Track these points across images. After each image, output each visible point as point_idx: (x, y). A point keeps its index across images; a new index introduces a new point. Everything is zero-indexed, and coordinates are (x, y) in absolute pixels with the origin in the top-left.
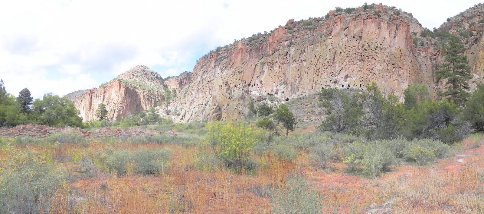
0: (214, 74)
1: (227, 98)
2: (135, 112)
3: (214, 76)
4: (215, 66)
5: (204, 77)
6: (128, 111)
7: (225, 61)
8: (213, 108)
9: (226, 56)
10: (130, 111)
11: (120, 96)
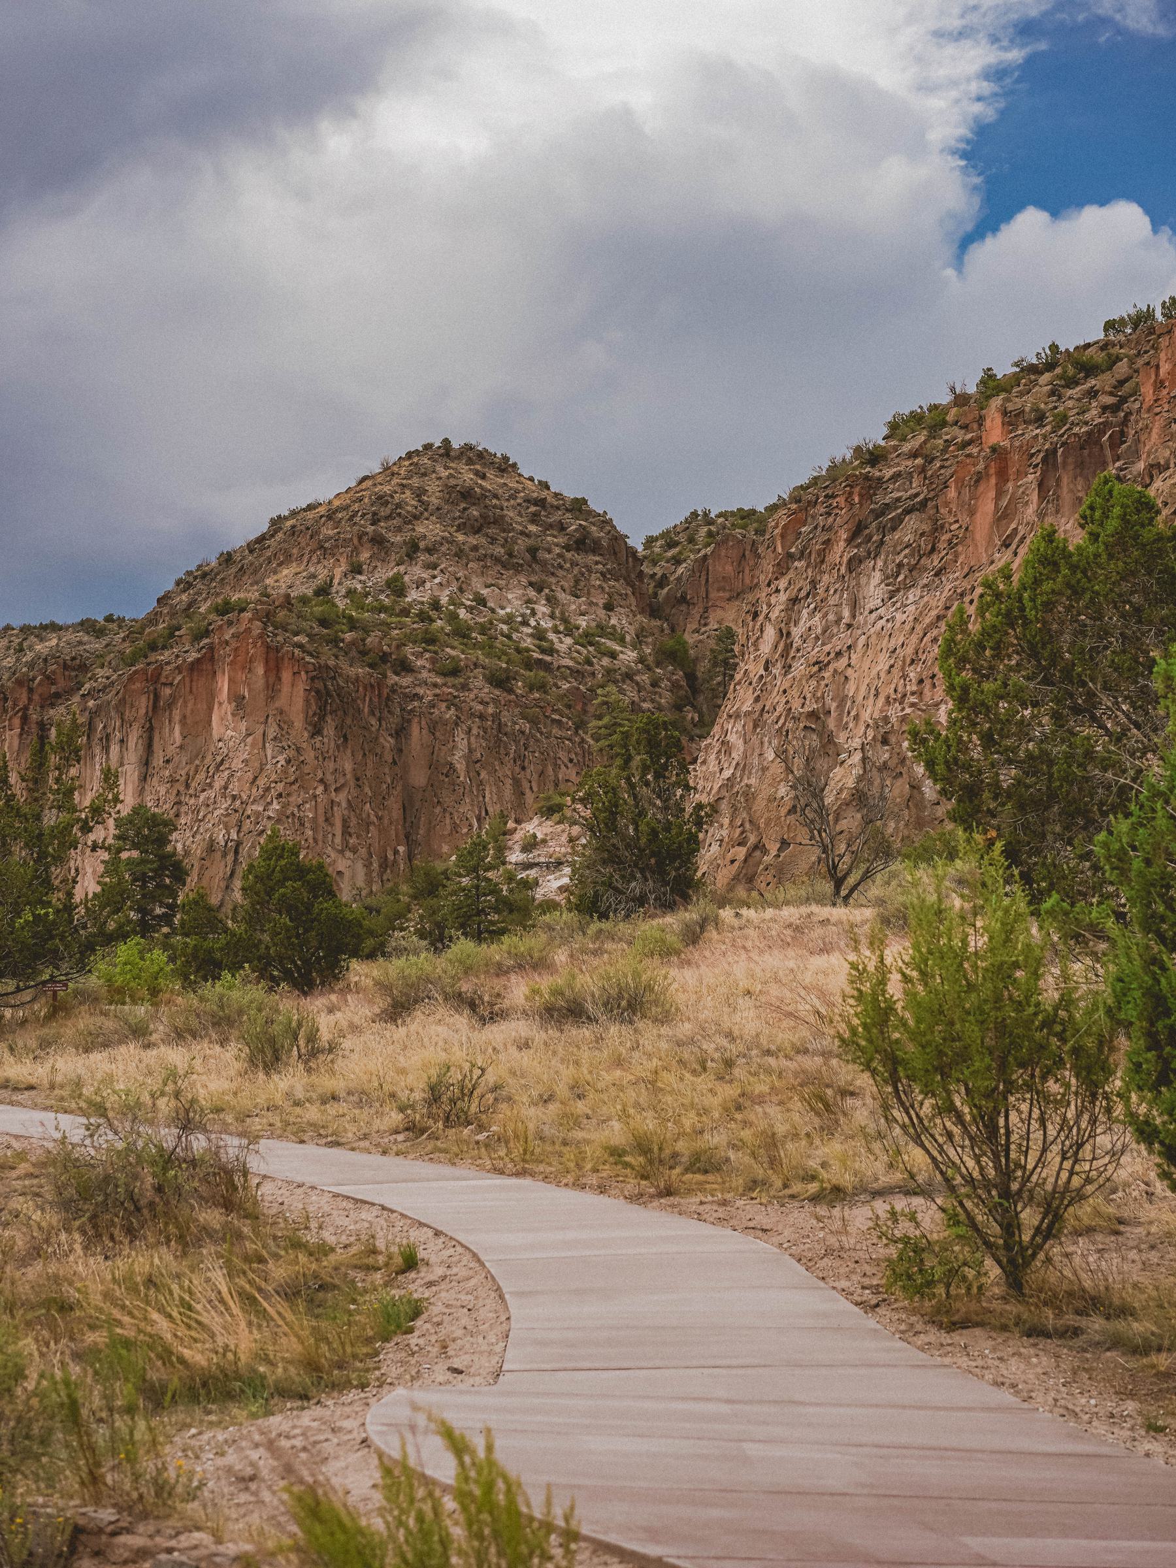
0: (846, 613)
1: (783, 811)
2: (396, 852)
3: (849, 626)
4: (854, 564)
5: (797, 632)
6: (341, 852)
7: (911, 528)
8: (732, 862)
9: (917, 495)
10: (354, 851)
11: (271, 736)
